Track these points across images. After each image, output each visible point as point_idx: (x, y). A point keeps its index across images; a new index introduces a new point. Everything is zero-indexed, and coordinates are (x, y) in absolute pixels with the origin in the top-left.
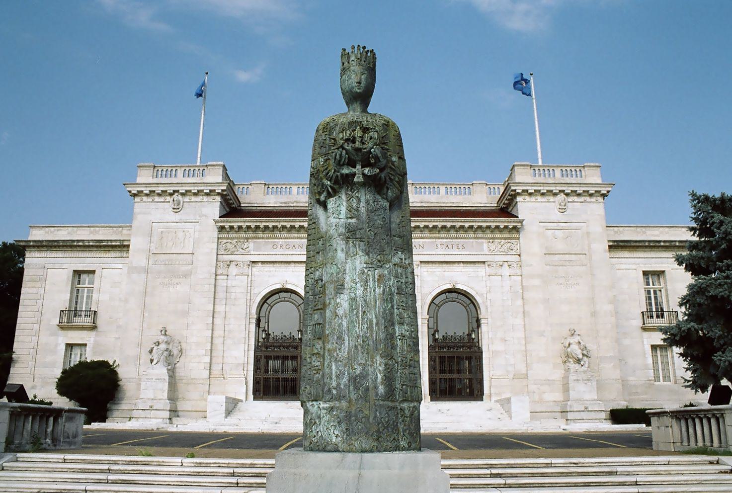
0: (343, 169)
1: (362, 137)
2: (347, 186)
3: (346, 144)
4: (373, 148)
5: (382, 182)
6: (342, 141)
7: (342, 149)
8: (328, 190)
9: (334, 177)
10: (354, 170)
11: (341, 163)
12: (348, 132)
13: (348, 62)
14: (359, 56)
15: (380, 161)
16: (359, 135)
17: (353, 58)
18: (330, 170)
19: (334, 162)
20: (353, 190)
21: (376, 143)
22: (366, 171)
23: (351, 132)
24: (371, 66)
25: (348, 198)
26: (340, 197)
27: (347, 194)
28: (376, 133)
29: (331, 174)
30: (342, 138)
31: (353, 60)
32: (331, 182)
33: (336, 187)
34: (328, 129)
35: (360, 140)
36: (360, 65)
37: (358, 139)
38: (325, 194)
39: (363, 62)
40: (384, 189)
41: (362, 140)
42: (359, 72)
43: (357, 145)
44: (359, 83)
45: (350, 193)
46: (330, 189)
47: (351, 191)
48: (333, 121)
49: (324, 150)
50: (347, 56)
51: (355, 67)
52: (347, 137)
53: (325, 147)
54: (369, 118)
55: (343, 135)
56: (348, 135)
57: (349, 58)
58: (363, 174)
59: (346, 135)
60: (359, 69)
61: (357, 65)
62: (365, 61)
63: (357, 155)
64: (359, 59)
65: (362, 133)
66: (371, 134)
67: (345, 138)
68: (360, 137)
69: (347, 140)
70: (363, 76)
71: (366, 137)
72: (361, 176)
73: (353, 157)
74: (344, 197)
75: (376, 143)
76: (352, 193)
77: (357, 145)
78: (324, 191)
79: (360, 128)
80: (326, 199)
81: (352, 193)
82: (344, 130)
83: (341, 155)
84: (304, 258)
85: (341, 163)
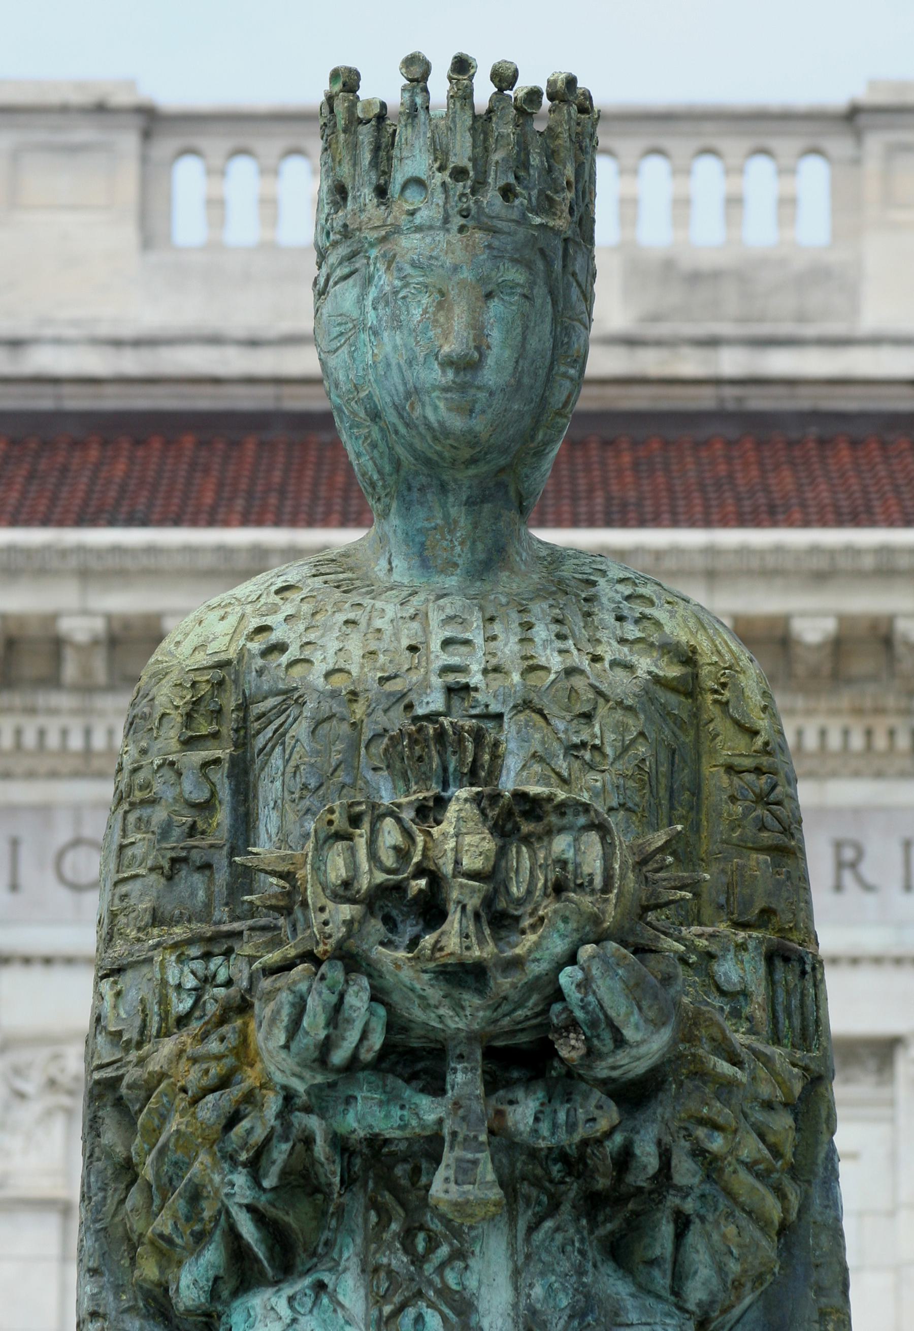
0: (350, 1100)
1: (492, 876)
2: (373, 1204)
3: (376, 926)
4: (572, 959)
5: (639, 1178)
6: (346, 911)
7: (348, 970)
8: (233, 1234)
9: (280, 1152)
10: (430, 1110)
11: (339, 1056)
12: (390, 835)
13: (381, 192)
14: (462, 151)
15: (620, 1042)
16: (470, 862)
17: (414, 161)
18: (249, 1098)
19: (286, 1047)
20: (421, 1246)
21: (596, 920)
22: (523, 1112)
23: (408, 835)
24: (561, 222)
25: (386, 1297)
26: (320, 1286)
27: (376, 1270)
28: (593, 837)
29: (257, 1125)
30: (346, 884)
31: (417, 182)
32: (256, 1180)
33: (293, 1219)
34: (231, 719)
35: (473, 902)
36: (471, 218)
37: (462, 895)
38: (212, 1256)
39: (491, 198)
40: (656, 1226)
41: (488, 901)
42: (466, 274)
43: (453, 943)
44: (466, 366)
45: (398, 1260)
46: (247, 1229)
47: (408, 1248)
48: (267, 652)
49: (193, 887)
50: (365, 134)
51: (426, 233)
52: (380, 877)
53: (207, 867)
54: (541, 632)
55: (353, 865)
56: (389, 859)
57: (384, 152)
58: (499, 1135)
59: (373, 856)
60: (460, 255)
61: (446, 220)
62: (507, 193)
63: (458, 1007)
64: (459, 174)
65: (489, 845)
66: (561, 844)
67: (364, 883)
68: (473, 875)
69: (384, 902)
70: (495, 307)
71: (525, 870)
72: (484, 1156)
73: (418, 1014)
74: (351, 1291)
75: (596, 920)
76: (418, 1260)
77: (454, 937)
78: (201, 1238)
79: (477, 799)
80: (214, 1294)
81: (418, 1260)
82: (355, 820)
83: (336, 1013)
84: (85, 938)
85: (339, 1056)
